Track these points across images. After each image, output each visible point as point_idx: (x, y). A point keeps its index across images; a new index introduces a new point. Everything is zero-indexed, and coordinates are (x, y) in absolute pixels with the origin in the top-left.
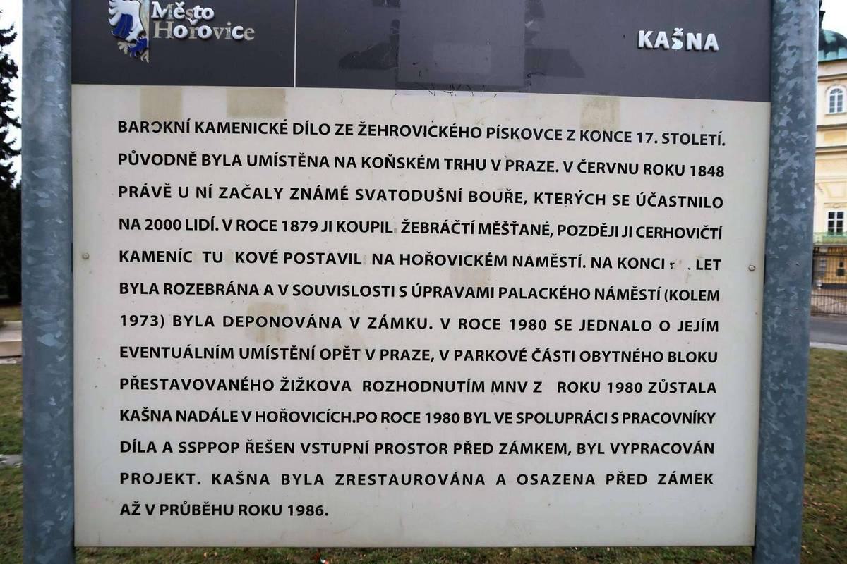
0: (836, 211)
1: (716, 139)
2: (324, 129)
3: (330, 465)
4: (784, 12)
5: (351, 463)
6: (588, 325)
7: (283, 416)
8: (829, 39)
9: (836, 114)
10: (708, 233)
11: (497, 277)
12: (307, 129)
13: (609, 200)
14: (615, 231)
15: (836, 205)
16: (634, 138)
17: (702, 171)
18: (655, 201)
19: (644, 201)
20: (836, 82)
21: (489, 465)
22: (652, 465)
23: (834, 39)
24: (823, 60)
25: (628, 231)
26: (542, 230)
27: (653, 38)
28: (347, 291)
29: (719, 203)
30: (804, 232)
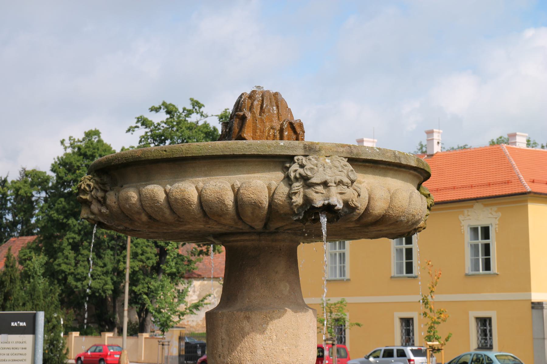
1: (25, 342)
4: (65, 309)
10: (24, 360)
13: (6, 355)
14: (7, 360)
16: (10, 343)
17: (22, 348)
18: (14, 354)
19: (12, 354)
24: (330, 278)
25: (9, 360)
27: (14, 324)
29: (25, 354)
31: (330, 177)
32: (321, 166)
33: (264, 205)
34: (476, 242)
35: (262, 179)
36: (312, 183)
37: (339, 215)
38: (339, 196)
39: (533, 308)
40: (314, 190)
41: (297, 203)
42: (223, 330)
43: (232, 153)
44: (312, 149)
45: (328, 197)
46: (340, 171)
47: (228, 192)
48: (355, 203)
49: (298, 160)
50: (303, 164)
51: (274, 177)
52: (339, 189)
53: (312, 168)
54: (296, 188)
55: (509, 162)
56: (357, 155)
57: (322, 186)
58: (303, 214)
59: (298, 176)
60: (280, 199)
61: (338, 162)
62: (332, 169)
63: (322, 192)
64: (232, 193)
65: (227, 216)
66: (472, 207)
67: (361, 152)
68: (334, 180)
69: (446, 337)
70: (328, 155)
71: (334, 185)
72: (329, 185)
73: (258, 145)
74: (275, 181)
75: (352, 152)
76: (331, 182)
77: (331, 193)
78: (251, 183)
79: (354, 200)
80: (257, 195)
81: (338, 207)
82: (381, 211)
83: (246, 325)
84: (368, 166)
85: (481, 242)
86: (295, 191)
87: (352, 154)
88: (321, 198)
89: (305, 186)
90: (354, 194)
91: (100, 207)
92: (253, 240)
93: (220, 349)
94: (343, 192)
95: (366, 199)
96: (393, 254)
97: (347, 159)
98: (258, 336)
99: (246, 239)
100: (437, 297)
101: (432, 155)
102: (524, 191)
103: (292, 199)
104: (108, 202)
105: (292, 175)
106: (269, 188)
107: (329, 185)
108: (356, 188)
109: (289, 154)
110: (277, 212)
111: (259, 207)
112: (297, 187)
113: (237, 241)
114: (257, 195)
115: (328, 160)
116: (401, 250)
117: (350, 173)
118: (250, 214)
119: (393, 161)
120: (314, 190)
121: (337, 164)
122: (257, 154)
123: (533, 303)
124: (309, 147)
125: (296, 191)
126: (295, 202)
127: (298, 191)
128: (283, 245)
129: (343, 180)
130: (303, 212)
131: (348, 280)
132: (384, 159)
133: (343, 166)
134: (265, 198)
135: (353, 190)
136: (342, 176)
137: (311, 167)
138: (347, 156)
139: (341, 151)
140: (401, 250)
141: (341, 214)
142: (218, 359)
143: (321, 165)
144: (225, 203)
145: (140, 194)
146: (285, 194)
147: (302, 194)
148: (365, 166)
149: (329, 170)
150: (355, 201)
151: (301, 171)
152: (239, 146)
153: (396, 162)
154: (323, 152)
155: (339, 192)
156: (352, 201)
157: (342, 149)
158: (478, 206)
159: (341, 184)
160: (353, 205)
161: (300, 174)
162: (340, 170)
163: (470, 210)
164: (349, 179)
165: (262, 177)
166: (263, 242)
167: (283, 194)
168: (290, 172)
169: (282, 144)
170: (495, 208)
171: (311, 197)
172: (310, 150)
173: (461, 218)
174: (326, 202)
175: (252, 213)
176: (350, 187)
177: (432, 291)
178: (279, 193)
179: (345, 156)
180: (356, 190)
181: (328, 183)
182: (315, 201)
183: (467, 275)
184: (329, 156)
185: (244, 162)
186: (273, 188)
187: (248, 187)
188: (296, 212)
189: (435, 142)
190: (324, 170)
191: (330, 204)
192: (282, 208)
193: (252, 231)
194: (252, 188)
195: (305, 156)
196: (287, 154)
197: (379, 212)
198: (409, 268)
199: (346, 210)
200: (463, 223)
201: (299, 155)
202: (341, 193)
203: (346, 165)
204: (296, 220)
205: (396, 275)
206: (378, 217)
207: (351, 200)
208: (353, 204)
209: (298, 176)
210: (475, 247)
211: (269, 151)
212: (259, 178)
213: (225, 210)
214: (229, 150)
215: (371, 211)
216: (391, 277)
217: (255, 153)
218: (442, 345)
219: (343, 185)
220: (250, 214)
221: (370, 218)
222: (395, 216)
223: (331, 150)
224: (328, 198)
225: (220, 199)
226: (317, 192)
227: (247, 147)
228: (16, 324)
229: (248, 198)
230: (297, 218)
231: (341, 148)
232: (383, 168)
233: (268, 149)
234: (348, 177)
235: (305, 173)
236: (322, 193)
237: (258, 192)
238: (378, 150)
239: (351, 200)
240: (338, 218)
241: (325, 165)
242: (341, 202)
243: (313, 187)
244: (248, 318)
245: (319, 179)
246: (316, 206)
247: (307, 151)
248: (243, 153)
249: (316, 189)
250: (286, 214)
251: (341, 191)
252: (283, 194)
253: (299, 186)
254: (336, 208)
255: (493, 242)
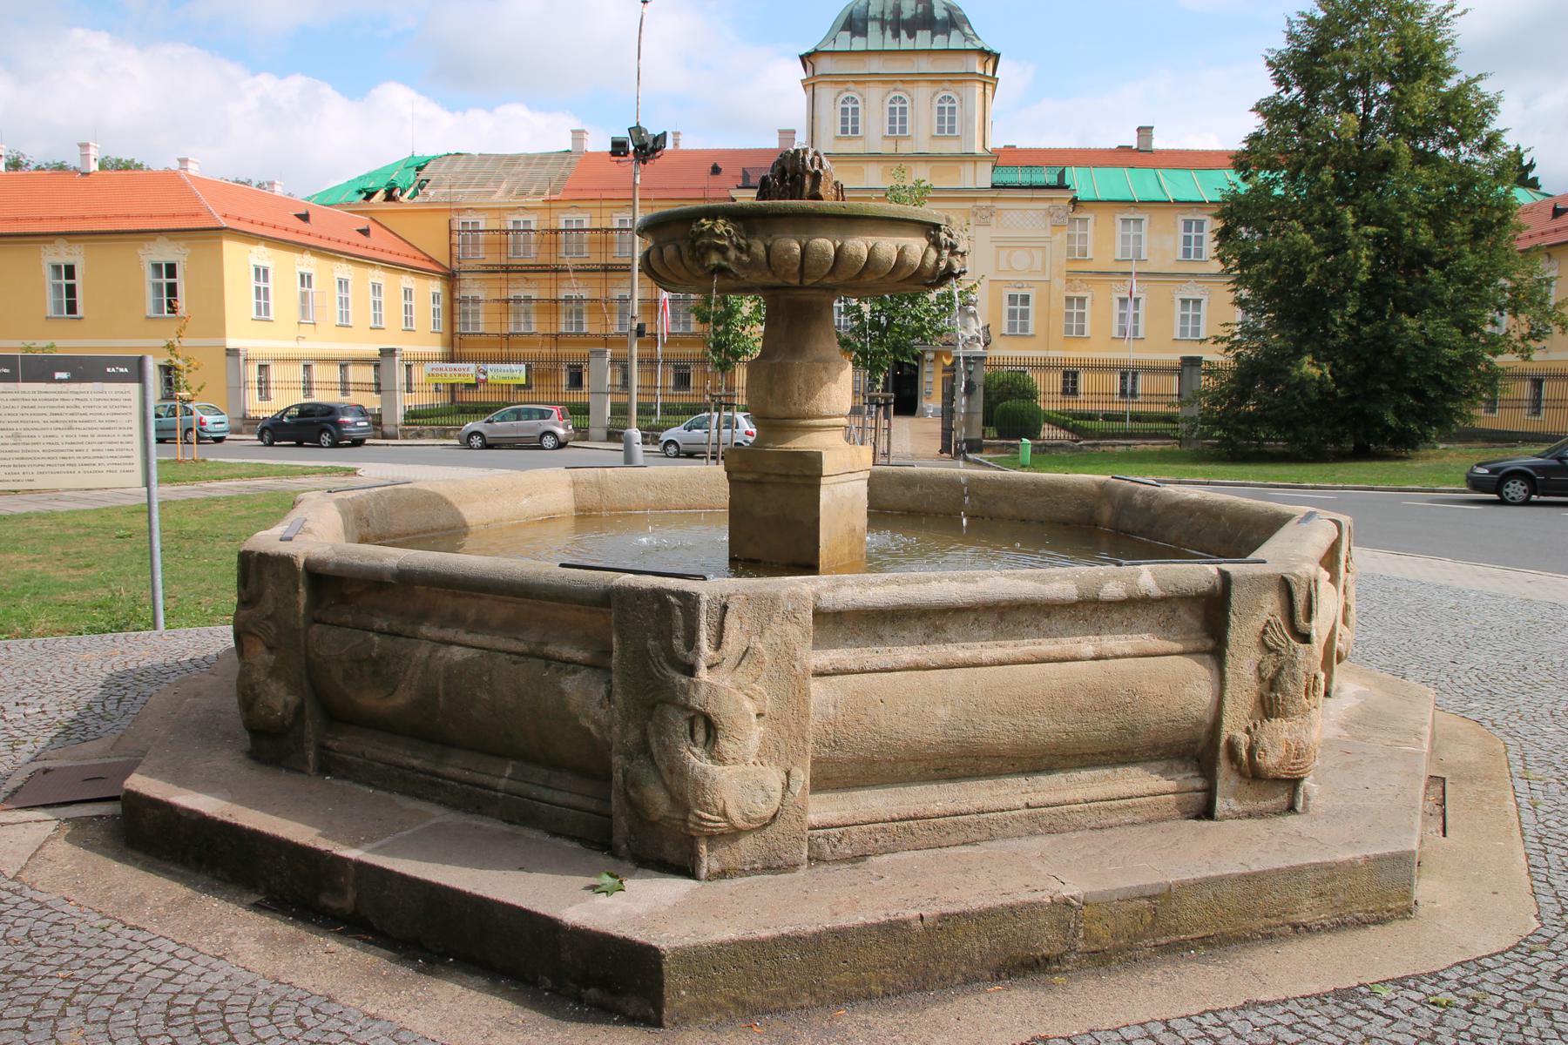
0: (1019, 292)
2: (29, 392)
3: (35, 470)
5: (41, 469)
6: (99, 436)
7: (22, 458)
8: (940, 13)
9: (850, 138)
11: (74, 425)
12: (24, 392)
15: (1020, 284)
20: (946, 85)
21: (77, 469)
22: (118, 468)
23: (945, 14)
26: (85, 414)
28: (37, 429)
30: (1411, 285)
34: (160, 280)
39: (227, 355)
42: (801, 380)
55: (192, 192)
66: (154, 240)
69: (199, 386)
83: (824, 376)
85: (165, 280)
91: (739, 255)
93: (796, 397)
96: (49, 291)
98: (833, 386)
100: (187, 342)
101: (88, 174)
102: (219, 226)
104: (753, 249)
116: (59, 286)
123: (227, 349)
131: (1032, 336)
140: (1015, 311)
142: (792, 407)
145: (768, 249)
158: (161, 239)
163: (152, 243)
170: (182, 243)
173: (140, 251)
177: (179, 336)
183: (1114, 338)
189: (92, 158)
198: (72, 308)
200: (142, 257)
205: (53, 315)
210: (158, 287)
216: (47, 318)
218: (193, 395)
228: (113, 370)
244: (826, 369)
255: (180, 281)
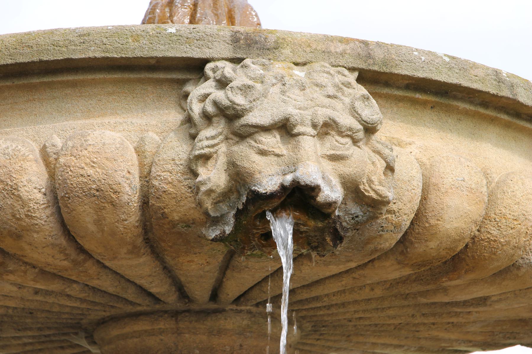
31: (300, 109)
32: (274, 81)
33: (126, 197)
35: (121, 128)
36: (247, 125)
37: (338, 226)
38: (328, 166)
40: (256, 145)
41: (209, 186)
43: (35, 59)
44: (256, 43)
45: (294, 164)
46: (329, 96)
47: (26, 165)
48: (378, 187)
49: (214, 70)
50: (225, 77)
51: (154, 123)
52: (328, 145)
53: (249, 87)
54: (206, 143)
56: (385, 63)
57: (278, 137)
58: (232, 221)
59: (210, 109)
60: (166, 179)
61: (325, 75)
62: (308, 91)
63: (277, 151)
64: (44, 168)
65: (35, 235)
67: (397, 58)
68: (310, 118)
70: (299, 60)
71: (310, 130)
72: (295, 131)
73: (107, 35)
74: (157, 133)
75: (369, 56)
76: (302, 124)
77: (302, 152)
78: (88, 138)
79: (373, 178)
80: (104, 169)
81: (328, 196)
82: (464, 226)
84: (424, 104)
86: (203, 151)
87: (371, 61)
88: (275, 169)
89: (231, 136)
90: (373, 163)
92: (161, 332)
94: (338, 153)
95: (415, 183)
97: (356, 74)
99: (146, 331)
103: (195, 175)
105: (196, 108)
106: (139, 152)
107: (295, 131)
108: (379, 147)
109: (190, 55)
110: (164, 216)
111: (112, 203)
112: (207, 139)
113: (125, 337)
114: (104, 169)
115: (299, 73)
117: (358, 105)
118: (92, 228)
119: (493, 91)
120: (256, 145)
121: (323, 79)
122: (103, 58)
124: (246, 39)
125: (206, 151)
126: (203, 183)
127: (212, 150)
128: (241, 346)
129: (337, 119)
130: (233, 212)
132: (465, 83)
133: (341, 86)
134: (128, 175)
135: (372, 154)
136: (334, 109)
137: (245, 83)
138: (355, 66)
139: (338, 50)
141: (344, 224)
143: (276, 78)
144: (19, 196)
146: (177, 162)
147: (221, 161)
148: (414, 102)
149: (297, 91)
150: (376, 183)
151: (220, 95)
152: (56, 38)
153: (501, 94)
154: (287, 51)
155: (328, 153)
156: (370, 181)
157: (340, 48)
159: (333, 133)
160: (372, 194)
161: (215, 103)
162: (331, 93)
164: (356, 118)
165: (121, 123)
166: (187, 335)
167: (175, 164)
168: (191, 100)
169: (172, 30)
171: (246, 165)
172: (249, 46)
174: (289, 178)
175: (98, 222)
176: (360, 144)
178: (164, 160)
179: (351, 65)
180: (379, 153)
181: (295, 126)
182: (258, 176)
184: (304, 64)
185: (74, 85)
186: (149, 148)
187: (80, 149)
188: (212, 214)
190: (283, 92)
191: (298, 182)
192: (173, 202)
193: (158, 307)
194: (90, 149)
195: (237, 61)
196: (184, 55)
197: (456, 225)
199: (355, 209)
201: (218, 59)
202: (334, 158)
203: (350, 84)
204: (214, 240)
206: (455, 241)
207: (365, 181)
208: (374, 190)
209: (210, 109)
211: (135, 49)
212: (114, 128)
213: (23, 216)
214: (29, 50)
215: (433, 222)
217: (96, 55)
219: (340, 133)
220: (92, 228)
221: (433, 244)
222: (508, 243)
223: (309, 46)
224: (293, 166)
225: (7, 184)
226: (263, 153)
227: (77, 41)
229: (81, 178)
230: (218, 232)
231: (339, 44)
232: (467, 113)
233: (132, 44)
234: (354, 112)
235: (228, 98)
236: (278, 156)
237: (107, 159)
238: (447, 59)
239: (365, 181)
240: (338, 238)
241: (286, 79)
242: (336, 182)
243: (252, 139)
245: (268, 114)
246: (262, 190)
247: (240, 48)
248: (66, 56)
249: (260, 142)
250: (189, 224)
251: (332, 152)
252: (175, 164)
253: (213, 138)
254: (321, 198)
